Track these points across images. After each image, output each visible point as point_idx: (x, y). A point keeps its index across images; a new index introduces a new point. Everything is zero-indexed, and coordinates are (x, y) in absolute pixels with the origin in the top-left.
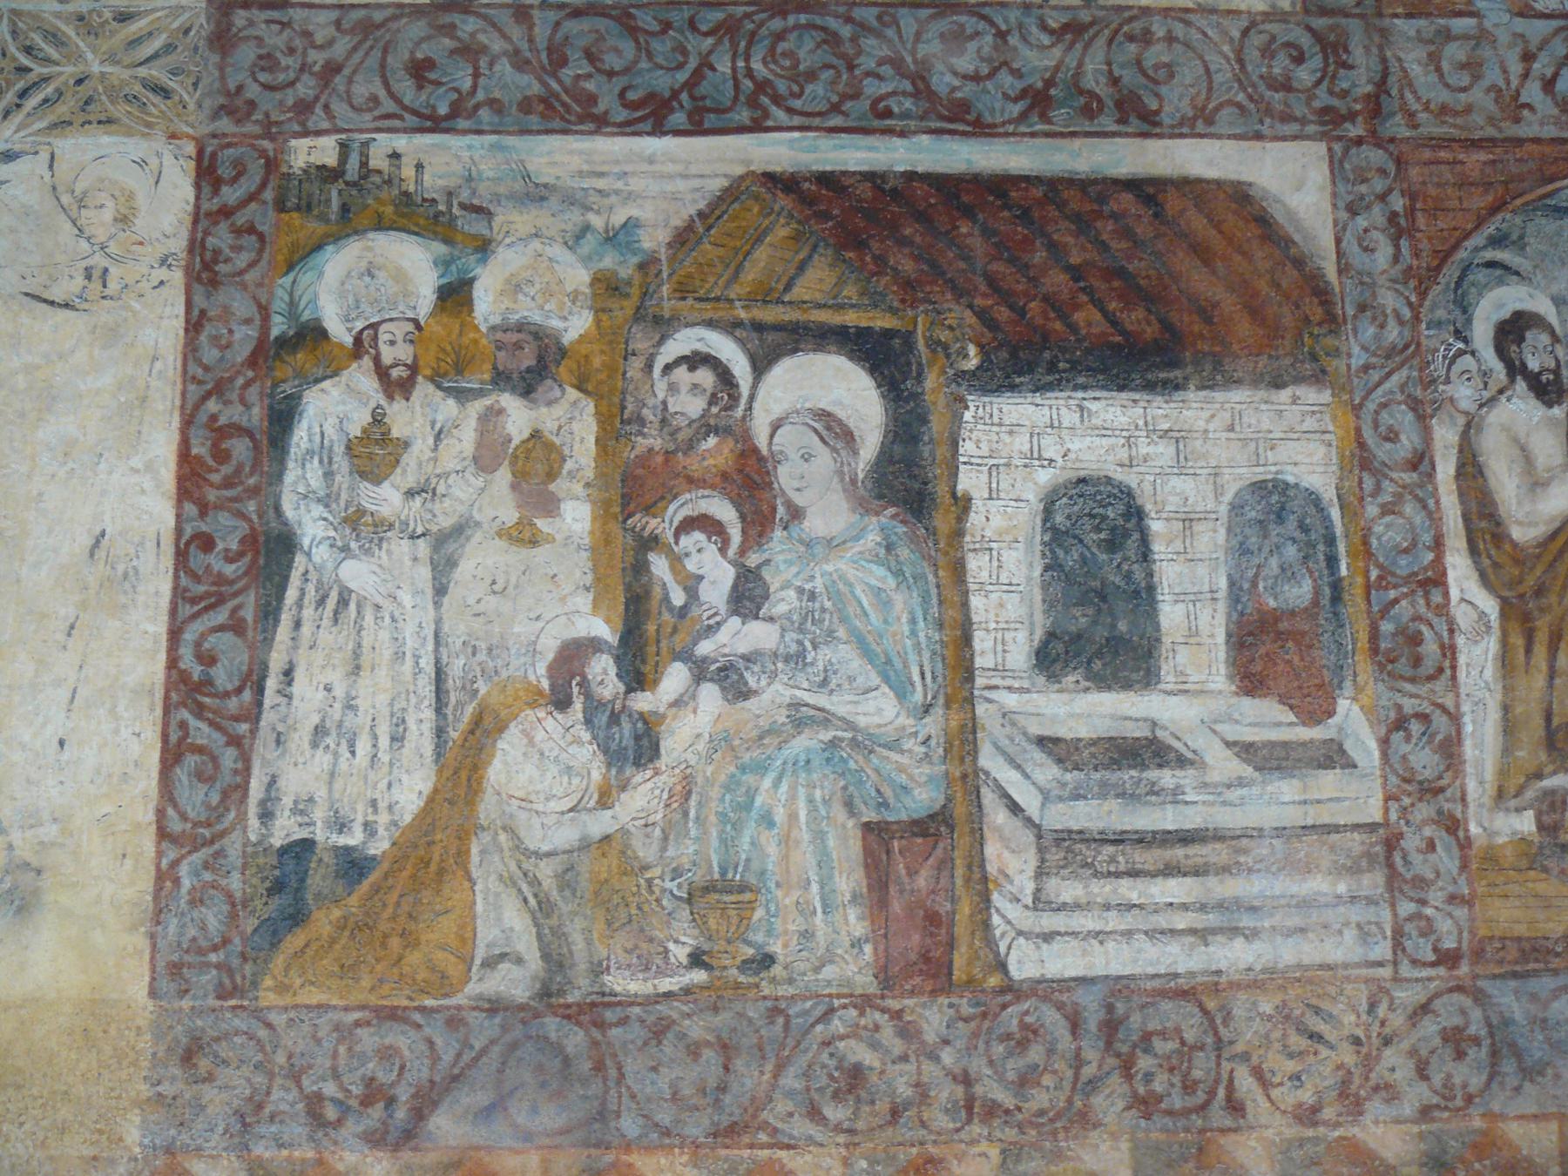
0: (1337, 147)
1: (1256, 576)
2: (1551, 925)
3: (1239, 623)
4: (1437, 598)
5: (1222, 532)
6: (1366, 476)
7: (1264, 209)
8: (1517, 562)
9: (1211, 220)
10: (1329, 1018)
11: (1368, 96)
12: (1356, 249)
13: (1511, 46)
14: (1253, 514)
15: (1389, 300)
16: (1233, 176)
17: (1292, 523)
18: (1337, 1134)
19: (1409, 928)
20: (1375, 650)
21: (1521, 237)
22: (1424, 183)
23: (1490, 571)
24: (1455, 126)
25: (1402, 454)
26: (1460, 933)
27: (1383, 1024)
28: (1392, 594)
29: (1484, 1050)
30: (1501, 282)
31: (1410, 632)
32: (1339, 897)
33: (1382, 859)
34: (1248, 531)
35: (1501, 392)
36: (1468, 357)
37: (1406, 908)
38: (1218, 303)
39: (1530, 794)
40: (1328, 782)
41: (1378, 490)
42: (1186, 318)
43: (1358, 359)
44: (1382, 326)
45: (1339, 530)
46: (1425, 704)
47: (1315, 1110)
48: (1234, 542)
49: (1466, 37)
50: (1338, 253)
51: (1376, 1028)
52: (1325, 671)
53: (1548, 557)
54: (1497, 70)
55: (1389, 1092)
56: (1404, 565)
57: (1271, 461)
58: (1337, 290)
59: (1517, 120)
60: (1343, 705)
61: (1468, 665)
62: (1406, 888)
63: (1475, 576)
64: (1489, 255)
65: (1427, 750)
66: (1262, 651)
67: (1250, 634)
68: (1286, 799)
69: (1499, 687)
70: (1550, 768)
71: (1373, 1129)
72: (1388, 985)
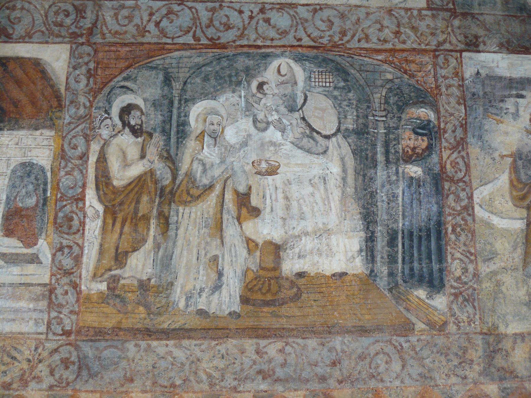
0: (74, 46)
1: (17, 195)
2: (107, 323)
3: (8, 211)
4: (80, 205)
5: (7, 180)
6: (62, 161)
7: (44, 67)
8: (114, 193)
9: (24, 72)
10: (20, 352)
11: (89, 28)
12: (73, 81)
13: (146, 10)
14: (19, 174)
15: (82, 99)
16: (35, 56)
17: (33, 177)
18: (17, 393)
19: (54, 321)
20: (55, 223)
21: (136, 77)
22: (103, 59)
23: (102, 196)
24: (119, 38)
25: (78, 154)
26: (72, 324)
27: (40, 355)
28: (65, 203)
29: (76, 367)
30: (125, 93)
31: (69, 217)
32: (30, 309)
33: (47, 296)
34: (16, 180)
35: (119, 132)
36: (109, 120)
37: (54, 314)
38: (21, 100)
39: (106, 276)
40: (31, 268)
41: (66, 166)
42: (8, 106)
43: (68, 119)
44: (78, 109)
45: (49, 180)
46: (71, 242)
47: (10, 384)
48: (11, 183)
49: (130, 7)
50: (66, 83)
51: (37, 356)
52: (36, 230)
53: (127, 192)
54: (139, 19)
55: (38, 379)
56: (71, 193)
57: (29, 155)
58: (64, 96)
59: (143, 36)
60: (41, 241)
61: (89, 229)
62: (55, 307)
63: (97, 197)
64: (122, 84)
65: (69, 259)
66: (14, 221)
67: (11, 215)
68: (15, 273)
69: (100, 237)
70: (115, 267)
71: (31, 392)
72: (43, 341)
